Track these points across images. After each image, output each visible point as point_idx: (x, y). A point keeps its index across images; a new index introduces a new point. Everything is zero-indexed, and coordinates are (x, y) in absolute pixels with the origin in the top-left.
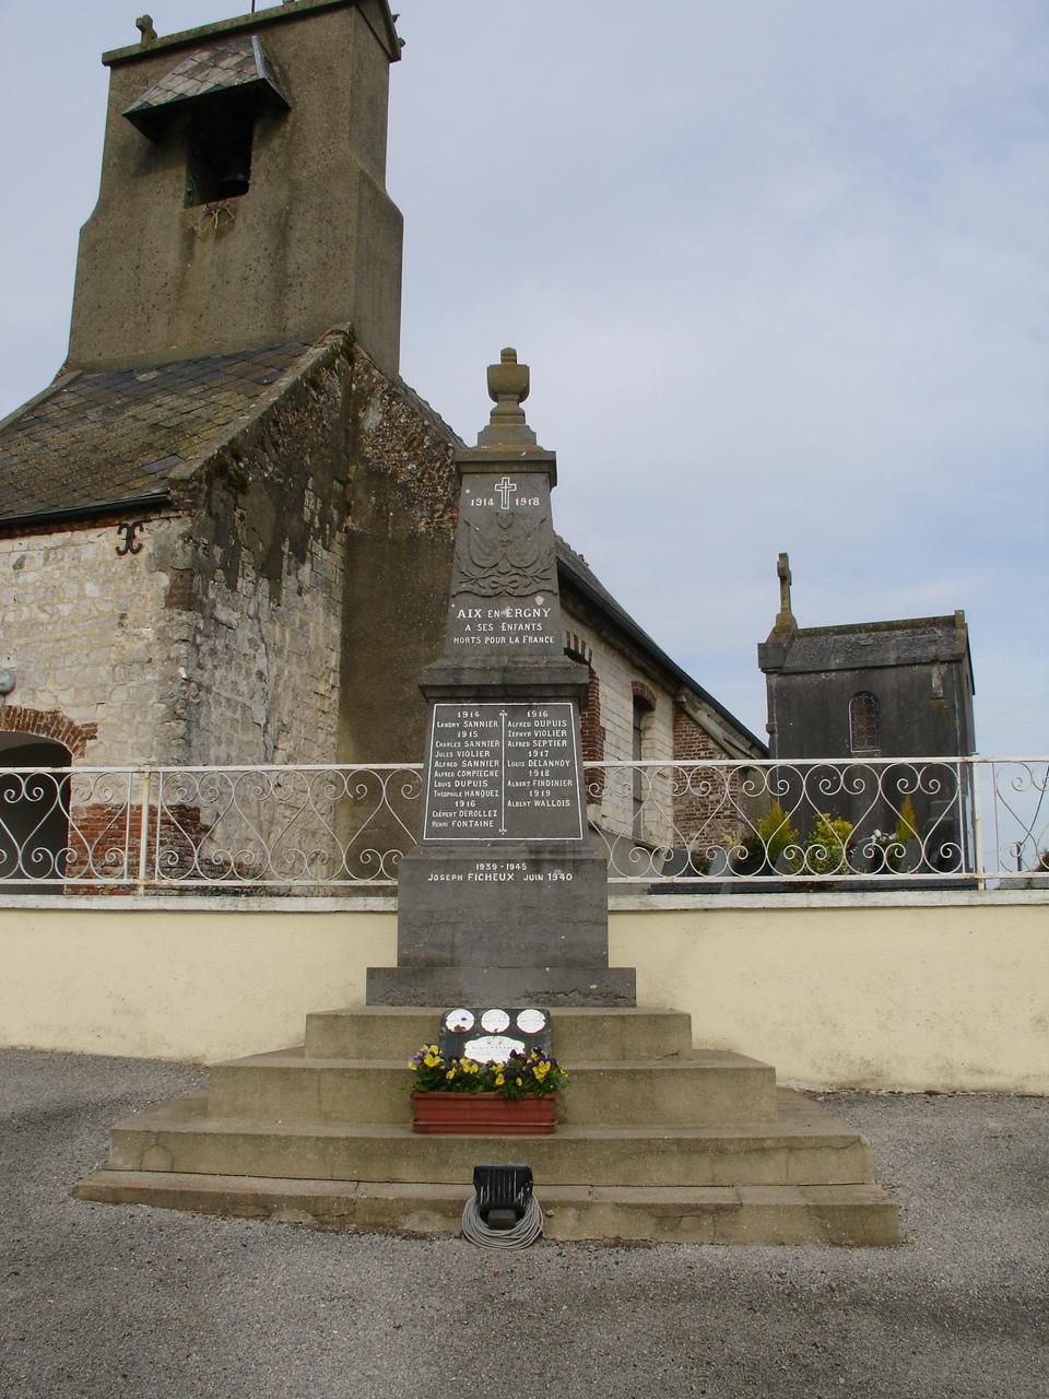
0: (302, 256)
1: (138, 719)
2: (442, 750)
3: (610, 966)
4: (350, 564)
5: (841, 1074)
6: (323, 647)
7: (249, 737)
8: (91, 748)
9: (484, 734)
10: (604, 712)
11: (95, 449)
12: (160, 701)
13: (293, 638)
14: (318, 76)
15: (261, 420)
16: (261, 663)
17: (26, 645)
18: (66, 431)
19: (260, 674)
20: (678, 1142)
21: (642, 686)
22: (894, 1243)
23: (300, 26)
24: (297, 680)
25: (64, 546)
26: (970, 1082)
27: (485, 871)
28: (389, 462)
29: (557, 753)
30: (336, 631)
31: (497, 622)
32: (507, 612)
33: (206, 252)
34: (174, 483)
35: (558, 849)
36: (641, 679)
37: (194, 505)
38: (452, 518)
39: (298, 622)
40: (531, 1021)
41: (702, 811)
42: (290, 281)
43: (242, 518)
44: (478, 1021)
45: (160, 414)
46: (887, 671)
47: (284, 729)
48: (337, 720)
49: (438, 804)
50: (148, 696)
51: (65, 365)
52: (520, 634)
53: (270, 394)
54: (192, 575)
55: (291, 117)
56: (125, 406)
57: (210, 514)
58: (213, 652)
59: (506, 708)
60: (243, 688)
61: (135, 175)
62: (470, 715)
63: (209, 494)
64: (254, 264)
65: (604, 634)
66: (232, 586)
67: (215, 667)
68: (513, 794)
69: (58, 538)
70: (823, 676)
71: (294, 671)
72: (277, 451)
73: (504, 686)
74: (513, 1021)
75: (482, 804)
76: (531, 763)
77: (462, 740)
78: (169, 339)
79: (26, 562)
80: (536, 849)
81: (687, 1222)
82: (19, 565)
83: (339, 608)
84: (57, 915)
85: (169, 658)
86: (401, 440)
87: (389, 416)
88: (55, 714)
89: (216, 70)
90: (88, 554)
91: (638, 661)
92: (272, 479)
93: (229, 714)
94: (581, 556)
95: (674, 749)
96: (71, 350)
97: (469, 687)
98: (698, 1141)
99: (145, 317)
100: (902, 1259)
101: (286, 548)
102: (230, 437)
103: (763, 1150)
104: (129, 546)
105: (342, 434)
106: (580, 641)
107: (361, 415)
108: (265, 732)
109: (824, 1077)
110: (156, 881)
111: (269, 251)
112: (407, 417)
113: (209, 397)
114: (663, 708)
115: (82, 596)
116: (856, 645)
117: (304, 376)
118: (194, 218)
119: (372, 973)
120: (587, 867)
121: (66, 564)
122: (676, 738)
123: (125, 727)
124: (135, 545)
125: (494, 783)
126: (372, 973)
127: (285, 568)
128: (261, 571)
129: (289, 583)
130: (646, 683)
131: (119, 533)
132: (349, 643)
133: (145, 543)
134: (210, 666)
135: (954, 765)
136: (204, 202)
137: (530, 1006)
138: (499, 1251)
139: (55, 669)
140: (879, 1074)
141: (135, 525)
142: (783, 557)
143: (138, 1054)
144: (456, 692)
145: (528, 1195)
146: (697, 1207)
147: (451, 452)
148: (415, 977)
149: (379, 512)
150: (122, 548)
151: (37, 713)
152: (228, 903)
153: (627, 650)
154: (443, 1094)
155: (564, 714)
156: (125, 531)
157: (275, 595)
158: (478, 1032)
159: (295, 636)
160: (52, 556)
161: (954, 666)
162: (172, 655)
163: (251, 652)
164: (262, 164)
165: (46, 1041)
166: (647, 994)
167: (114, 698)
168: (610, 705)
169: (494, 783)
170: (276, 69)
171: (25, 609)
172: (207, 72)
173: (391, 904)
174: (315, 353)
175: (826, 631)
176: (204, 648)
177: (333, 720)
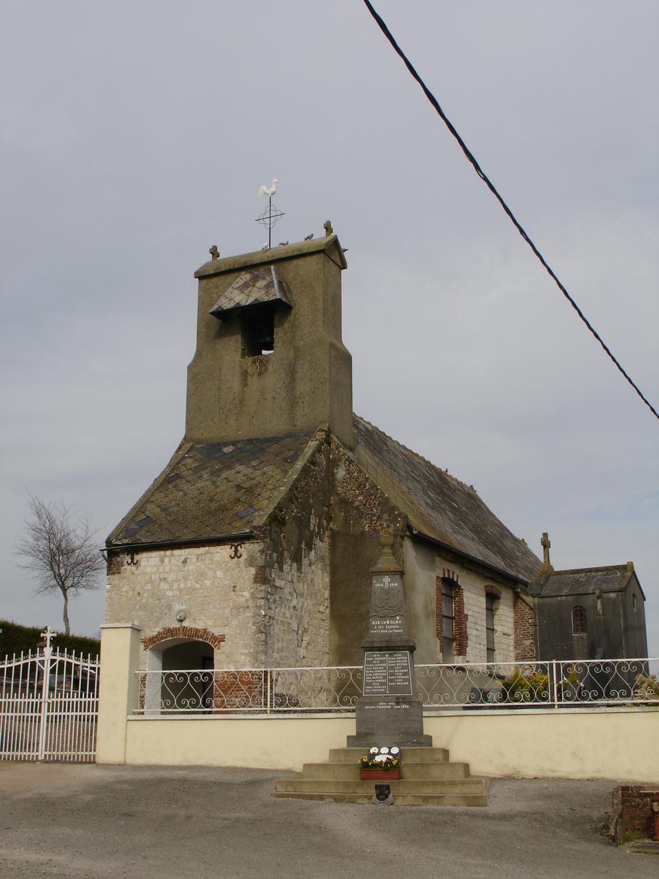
0: (302, 387)
1: (244, 633)
2: (369, 667)
3: (424, 734)
4: (333, 548)
5: (506, 771)
6: (321, 588)
7: (290, 637)
8: (223, 646)
9: (381, 662)
10: (466, 606)
11: (212, 500)
12: (254, 624)
13: (308, 588)
14: (306, 290)
15: (291, 490)
16: (295, 602)
17: (190, 598)
18: (194, 485)
19: (294, 607)
20: (432, 782)
21: (491, 587)
22: (485, 806)
23: (295, 262)
24: (310, 607)
25: (207, 553)
26: (550, 774)
27: (382, 705)
28: (350, 495)
29: (404, 668)
30: (327, 580)
31: (385, 626)
32: (388, 622)
33: (253, 382)
34: (255, 528)
35: (404, 698)
36: (490, 583)
37: (265, 537)
38: (381, 524)
39: (310, 580)
40: (395, 750)
41: (531, 653)
42: (297, 400)
43: (284, 537)
44: (379, 750)
45: (240, 478)
46: (589, 596)
47: (305, 631)
48: (328, 623)
49: (367, 684)
50: (248, 623)
51: (185, 439)
52: (392, 629)
53: (292, 474)
54: (266, 569)
55: (293, 312)
56: (220, 470)
57: (271, 539)
58: (275, 601)
59: (388, 654)
60: (288, 615)
61: (214, 338)
62: (377, 656)
63: (270, 531)
64: (278, 391)
65: (465, 565)
66: (281, 569)
67: (276, 608)
68: (391, 681)
69: (202, 550)
70: (559, 598)
71: (309, 603)
72: (298, 502)
73: (386, 647)
74: (390, 751)
75: (381, 684)
76: (396, 671)
77: (375, 664)
78: (237, 428)
79: (188, 560)
80: (398, 698)
81: (430, 800)
82: (185, 562)
83: (328, 568)
84: (170, 721)
85: (256, 606)
86: (355, 484)
87: (349, 472)
88: (205, 630)
89: (255, 289)
90: (217, 557)
91: (487, 574)
92: (296, 515)
93: (282, 627)
94: (471, 486)
95: (514, 618)
96: (187, 431)
97: (376, 647)
98: (437, 782)
99: (224, 416)
100: (487, 808)
101: (303, 546)
102: (277, 502)
103: (455, 784)
104: (236, 555)
105: (327, 482)
106: (451, 573)
107: (335, 471)
108: (297, 633)
109: (500, 773)
110: (274, 709)
111: (286, 383)
112: (358, 473)
113: (262, 469)
114: (506, 596)
115: (215, 577)
116: (577, 581)
117: (308, 461)
118: (247, 364)
119: (348, 737)
120: (413, 704)
121: (207, 561)
122: (515, 612)
123: (238, 636)
124: (239, 555)
125: (385, 677)
126: (348, 737)
127: (303, 555)
128: (294, 559)
129: (305, 562)
130: (494, 585)
131: (231, 548)
132: (334, 585)
133: (243, 554)
134: (274, 608)
135: (547, 664)
136: (253, 356)
137: (395, 746)
138: (381, 806)
139: (204, 610)
140: (518, 772)
141: (238, 545)
142: (545, 535)
143: (270, 768)
144: (372, 649)
145: (389, 793)
146: (432, 797)
147: (379, 491)
148: (361, 738)
149: (346, 521)
150: (233, 556)
151: (197, 630)
152: (300, 716)
153: (480, 571)
154: (368, 769)
155: (406, 655)
156: (233, 548)
157: (299, 569)
158: (379, 753)
159: (312, 583)
160: (200, 558)
161: (620, 593)
162: (258, 605)
163: (290, 598)
164: (279, 335)
165: (239, 764)
166: (437, 743)
167: (232, 623)
168: (471, 601)
169: (385, 677)
170: (284, 285)
171: (189, 582)
172: (249, 289)
173: (354, 715)
174: (313, 444)
175: (566, 572)
176: (271, 600)
177: (327, 623)
